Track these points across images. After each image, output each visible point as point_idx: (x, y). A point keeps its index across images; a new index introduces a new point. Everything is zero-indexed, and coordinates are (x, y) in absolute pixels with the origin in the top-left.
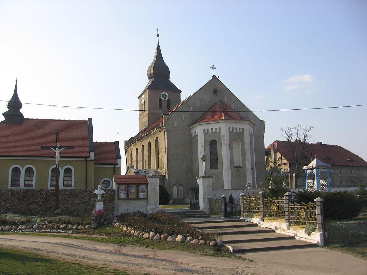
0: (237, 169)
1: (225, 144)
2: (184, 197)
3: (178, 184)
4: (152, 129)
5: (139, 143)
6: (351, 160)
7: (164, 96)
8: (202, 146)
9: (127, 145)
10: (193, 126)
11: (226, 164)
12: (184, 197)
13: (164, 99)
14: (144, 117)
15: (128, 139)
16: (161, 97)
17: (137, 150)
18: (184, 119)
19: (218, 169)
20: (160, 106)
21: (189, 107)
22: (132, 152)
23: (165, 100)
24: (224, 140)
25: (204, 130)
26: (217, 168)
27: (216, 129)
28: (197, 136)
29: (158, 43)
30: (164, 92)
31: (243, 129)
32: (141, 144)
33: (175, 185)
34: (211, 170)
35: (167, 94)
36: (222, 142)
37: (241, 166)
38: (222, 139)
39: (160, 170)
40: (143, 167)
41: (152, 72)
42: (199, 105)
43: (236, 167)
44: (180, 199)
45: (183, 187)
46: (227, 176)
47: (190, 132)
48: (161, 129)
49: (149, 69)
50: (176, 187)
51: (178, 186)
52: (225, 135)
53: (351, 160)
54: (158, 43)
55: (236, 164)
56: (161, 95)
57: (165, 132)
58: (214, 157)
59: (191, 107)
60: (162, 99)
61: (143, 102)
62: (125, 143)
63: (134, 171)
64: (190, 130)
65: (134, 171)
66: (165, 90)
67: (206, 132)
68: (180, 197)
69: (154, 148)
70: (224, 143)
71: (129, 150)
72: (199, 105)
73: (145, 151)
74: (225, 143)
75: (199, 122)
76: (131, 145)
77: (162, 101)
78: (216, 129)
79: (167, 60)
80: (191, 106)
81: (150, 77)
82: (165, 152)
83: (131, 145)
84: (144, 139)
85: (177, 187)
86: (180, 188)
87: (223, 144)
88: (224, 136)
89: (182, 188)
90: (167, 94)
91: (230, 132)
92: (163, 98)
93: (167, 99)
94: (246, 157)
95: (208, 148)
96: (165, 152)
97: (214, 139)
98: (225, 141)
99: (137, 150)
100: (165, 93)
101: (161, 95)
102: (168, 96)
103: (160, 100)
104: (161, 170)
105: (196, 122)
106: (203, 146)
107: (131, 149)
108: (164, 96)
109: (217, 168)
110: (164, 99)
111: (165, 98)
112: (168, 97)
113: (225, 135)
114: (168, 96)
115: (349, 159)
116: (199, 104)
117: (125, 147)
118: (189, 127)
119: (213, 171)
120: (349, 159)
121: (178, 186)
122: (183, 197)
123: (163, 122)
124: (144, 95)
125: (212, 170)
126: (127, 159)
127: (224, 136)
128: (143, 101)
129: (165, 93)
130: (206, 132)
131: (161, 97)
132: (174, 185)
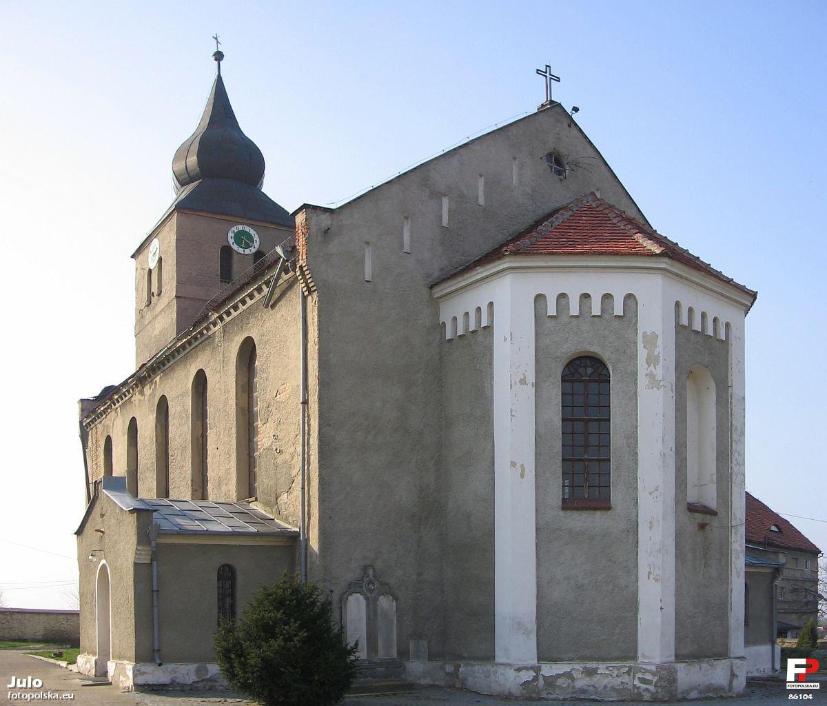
1: (654, 382)
2: (404, 653)
3: (371, 582)
4: (216, 309)
5: (142, 393)
8: (523, 382)
9: (88, 417)
10: (481, 272)
11: (657, 489)
12: (404, 653)
13: (241, 250)
15: (93, 392)
16: (231, 241)
17: (133, 426)
18: (407, 248)
19: (610, 512)
20: (226, 273)
21: (437, 195)
22: (109, 441)
23: (247, 251)
25: (540, 298)
26: (603, 504)
27: (607, 297)
28: (489, 329)
29: (219, 77)
30: (242, 224)
32: (153, 395)
33: (353, 587)
34: (569, 513)
35: (252, 232)
36: (642, 368)
37: (713, 504)
38: (642, 354)
39: (267, 504)
41: (193, 159)
42: (481, 201)
43: (693, 508)
44: (381, 664)
45: (396, 598)
46: (659, 551)
49: (182, 153)
50: (361, 598)
51: (371, 591)
54: (219, 77)
55: (692, 497)
56: (231, 234)
57: (305, 298)
59: (445, 202)
60: (235, 247)
61: (153, 264)
62: (82, 410)
63: (128, 505)
64: (435, 304)
65: (128, 505)
67: (552, 311)
68: (381, 654)
69: (226, 404)
70: (651, 376)
72: (481, 201)
75: (516, 253)
77: (235, 257)
78: (607, 297)
79: (251, 124)
80: (445, 195)
81: (183, 179)
82: (305, 402)
84: (172, 369)
85: (367, 599)
86: (386, 603)
87: (642, 381)
90: (252, 232)
92: (239, 245)
93: (253, 250)
94: (734, 462)
95: (554, 392)
96: (305, 402)
97: (595, 349)
98: (660, 366)
99: (133, 426)
101: (231, 234)
102: (256, 238)
103: (227, 252)
105: (493, 255)
106: (531, 378)
107: (107, 427)
109: (603, 504)
110: (241, 250)
111: (248, 246)
112: (257, 245)
113: (659, 333)
114: (256, 238)
116: (481, 193)
117: (81, 422)
118: (431, 288)
119: (580, 520)
121: (371, 591)
122: (394, 653)
123: (294, 248)
124: (160, 236)
125: (575, 514)
126: (90, 471)
127: (651, 340)
128: (153, 261)
130: (552, 311)
131: (231, 241)
132: (350, 586)
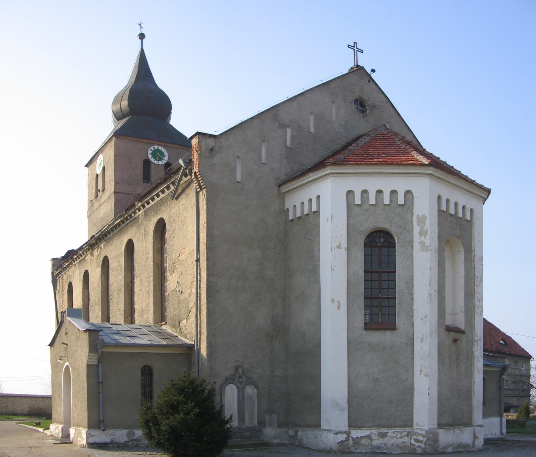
0: (453, 335)
2: (262, 423)
3: (240, 377)
4: (140, 200)
6: (504, 343)
7: (157, 154)
8: (339, 247)
9: (57, 270)
11: (426, 317)
12: (262, 423)
13: (156, 162)
14: (100, 206)
15: (61, 253)
16: (150, 156)
17: (86, 276)
18: (264, 160)
19: (395, 332)
21: (283, 126)
22: (70, 285)
23: (160, 163)
24: (422, 233)
25: (350, 193)
26: (392, 327)
27: (394, 192)
31: (472, 210)
32: (99, 256)
33: (229, 380)
34: (369, 332)
36: (417, 238)
38: (416, 229)
39: (173, 326)
40: (106, 317)
41: (125, 103)
43: (449, 329)
45: (256, 387)
47: (283, 203)
48: (179, 191)
49: (118, 99)
50: (234, 387)
51: (241, 383)
52: (427, 215)
53: (504, 343)
55: (449, 321)
56: (150, 152)
57: (197, 193)
58: (380, 288)
60: (152, 160)
64: (282, 197)
66: (160, 140)
67: (358, 201)
70: (422, 243)
71: (63, 281)
73: (112, 273)
74: (427, 244)
75: (335, 164)
76: (68, 266)
77: (153, 166)
81: (119, 116)
82: (198, 261)
83: (68, 266)
84: (111, 239)
85: (238, 388)
86: (250, 390)
88: (422, 220)
89: (256, 391)
90: (164, 150)
91: (440, 211)
94: (476, 299)
96: (198, 261)
99: (86, 276)
100: (160, 148)
101: (150, 152)
102: (166, 154)
103: (147, 163)
104: (177, 325)
106: (344, 245)
108: (157, 154)
109: (392, 327)
110: (156, 162)
111: (161, 159)
114: (166, 154)
115: (502, 342)
117: (53, 273)
118: (280, 186)
119: (375, 337)
120: (502, 342)
124: (104, 152)
125: (373, 333)
127: (422, 220)
128: (99, 169)
129: (160, 148)
130: (358, 201)
131: (150, 156)
